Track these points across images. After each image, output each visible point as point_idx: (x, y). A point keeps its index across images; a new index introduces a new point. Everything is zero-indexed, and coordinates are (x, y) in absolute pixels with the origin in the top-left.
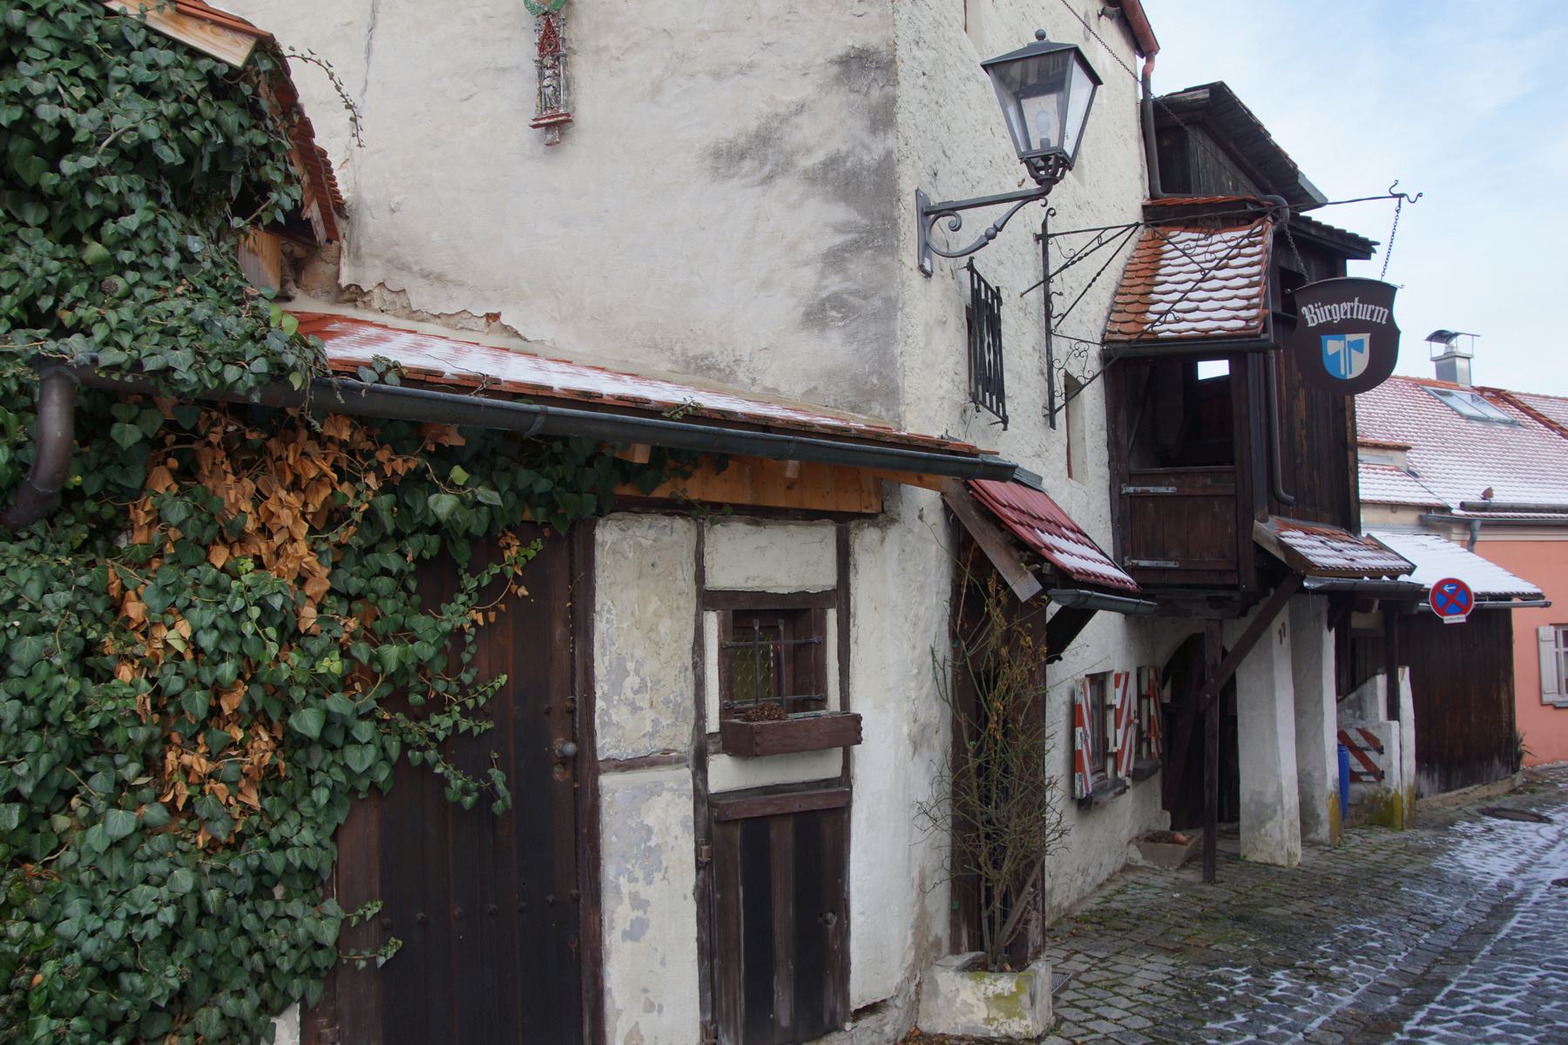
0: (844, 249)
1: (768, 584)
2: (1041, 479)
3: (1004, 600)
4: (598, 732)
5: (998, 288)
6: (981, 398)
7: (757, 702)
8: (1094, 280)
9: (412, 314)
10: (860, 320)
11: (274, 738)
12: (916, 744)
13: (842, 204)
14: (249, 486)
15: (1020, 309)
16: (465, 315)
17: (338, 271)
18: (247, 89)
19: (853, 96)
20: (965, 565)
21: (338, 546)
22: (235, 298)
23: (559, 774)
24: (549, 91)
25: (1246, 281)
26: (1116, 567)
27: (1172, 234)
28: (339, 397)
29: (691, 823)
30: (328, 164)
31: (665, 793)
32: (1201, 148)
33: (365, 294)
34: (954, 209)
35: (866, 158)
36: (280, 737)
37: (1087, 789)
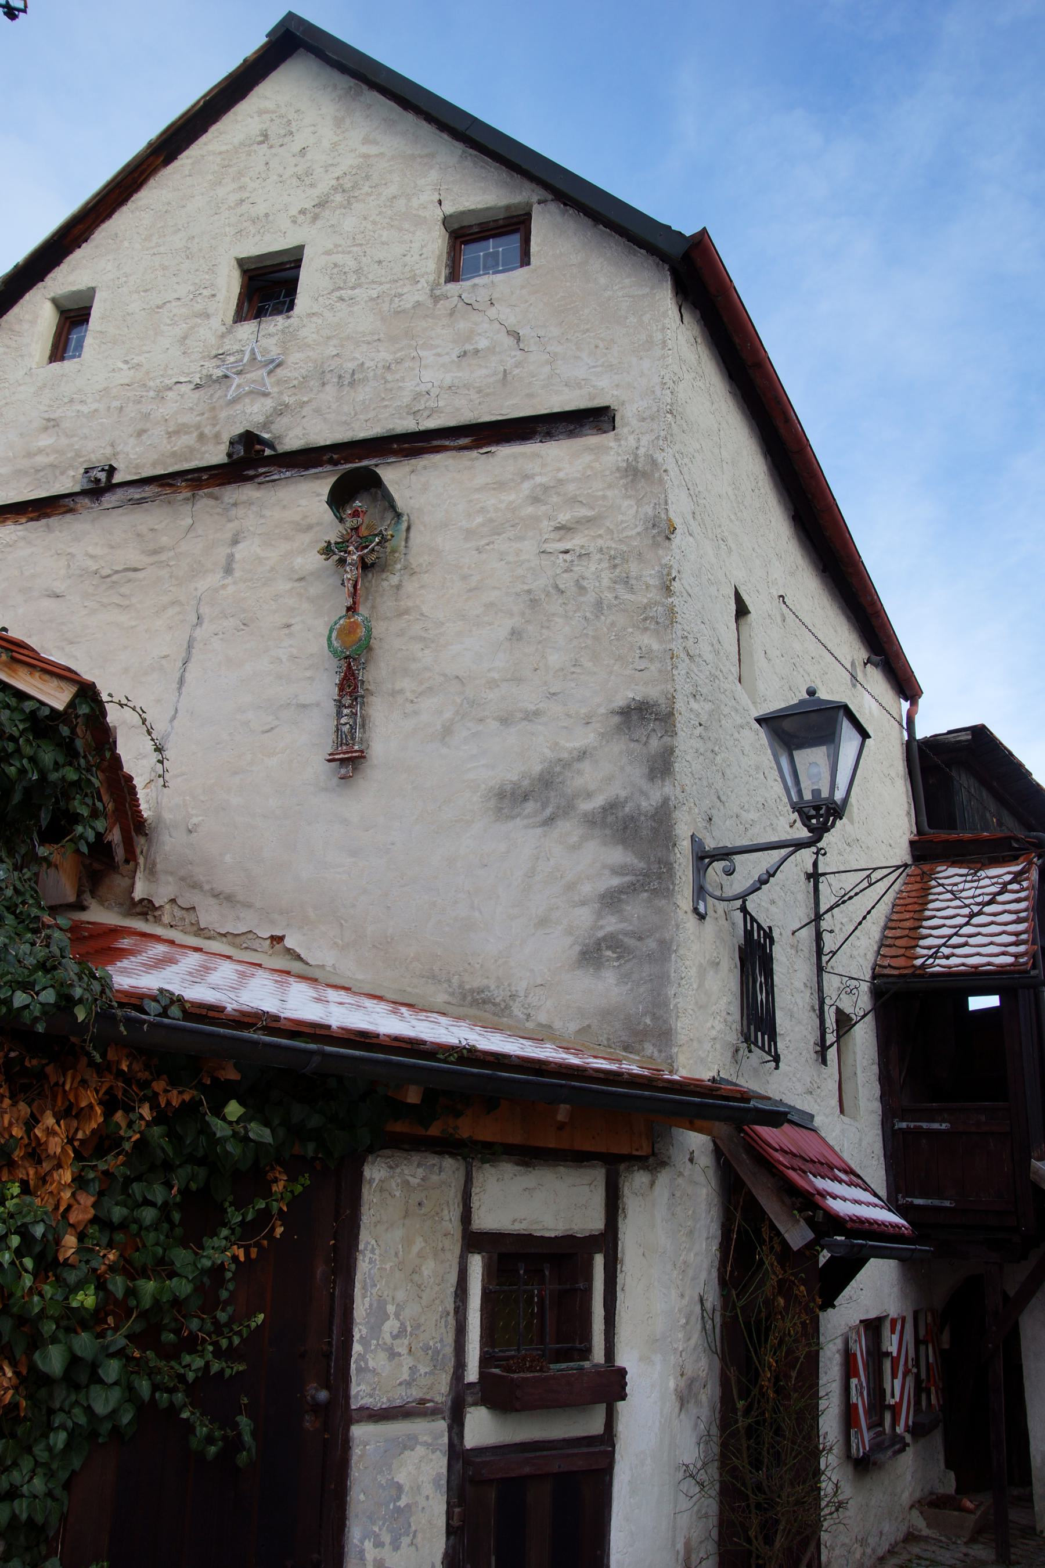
0: (621, 890)
1: (535, 1227)
2: (812, 1117)
3: (777, 1248)
4: (354, 1379)
5: (770, 928)
6: (753, 1039)
7: (518, 1350)
8: (864, 918)
9: (200, 931)
10: (635, 961)
11: (16, 1373)
12: (683, 1399)
13: (620, 848)
14: (24, 1109)
15: (792, 946)
16: (250, 936)
17: (133, 885)
18: (65, 731)
19: (632, 745)
20: (736, 1209)
21: (106, 1173)
22: (31, 926)
23: (309, 1423)
24: (346, 728)
25: (1013, 917)
26: (890, 1210)
27: (939, 869)
28: (122, 1028)
29: (444, 1482)
30: (134, 787)
31: (418, 1447)
32: (966, 786)
33: (157, 909)
34: (728, 854)
35: (644, 804)
36: (25, 1372)
37: (864, 1448)
